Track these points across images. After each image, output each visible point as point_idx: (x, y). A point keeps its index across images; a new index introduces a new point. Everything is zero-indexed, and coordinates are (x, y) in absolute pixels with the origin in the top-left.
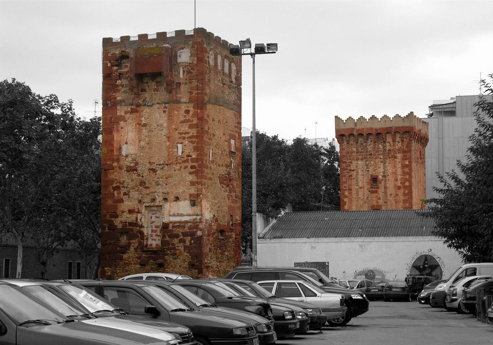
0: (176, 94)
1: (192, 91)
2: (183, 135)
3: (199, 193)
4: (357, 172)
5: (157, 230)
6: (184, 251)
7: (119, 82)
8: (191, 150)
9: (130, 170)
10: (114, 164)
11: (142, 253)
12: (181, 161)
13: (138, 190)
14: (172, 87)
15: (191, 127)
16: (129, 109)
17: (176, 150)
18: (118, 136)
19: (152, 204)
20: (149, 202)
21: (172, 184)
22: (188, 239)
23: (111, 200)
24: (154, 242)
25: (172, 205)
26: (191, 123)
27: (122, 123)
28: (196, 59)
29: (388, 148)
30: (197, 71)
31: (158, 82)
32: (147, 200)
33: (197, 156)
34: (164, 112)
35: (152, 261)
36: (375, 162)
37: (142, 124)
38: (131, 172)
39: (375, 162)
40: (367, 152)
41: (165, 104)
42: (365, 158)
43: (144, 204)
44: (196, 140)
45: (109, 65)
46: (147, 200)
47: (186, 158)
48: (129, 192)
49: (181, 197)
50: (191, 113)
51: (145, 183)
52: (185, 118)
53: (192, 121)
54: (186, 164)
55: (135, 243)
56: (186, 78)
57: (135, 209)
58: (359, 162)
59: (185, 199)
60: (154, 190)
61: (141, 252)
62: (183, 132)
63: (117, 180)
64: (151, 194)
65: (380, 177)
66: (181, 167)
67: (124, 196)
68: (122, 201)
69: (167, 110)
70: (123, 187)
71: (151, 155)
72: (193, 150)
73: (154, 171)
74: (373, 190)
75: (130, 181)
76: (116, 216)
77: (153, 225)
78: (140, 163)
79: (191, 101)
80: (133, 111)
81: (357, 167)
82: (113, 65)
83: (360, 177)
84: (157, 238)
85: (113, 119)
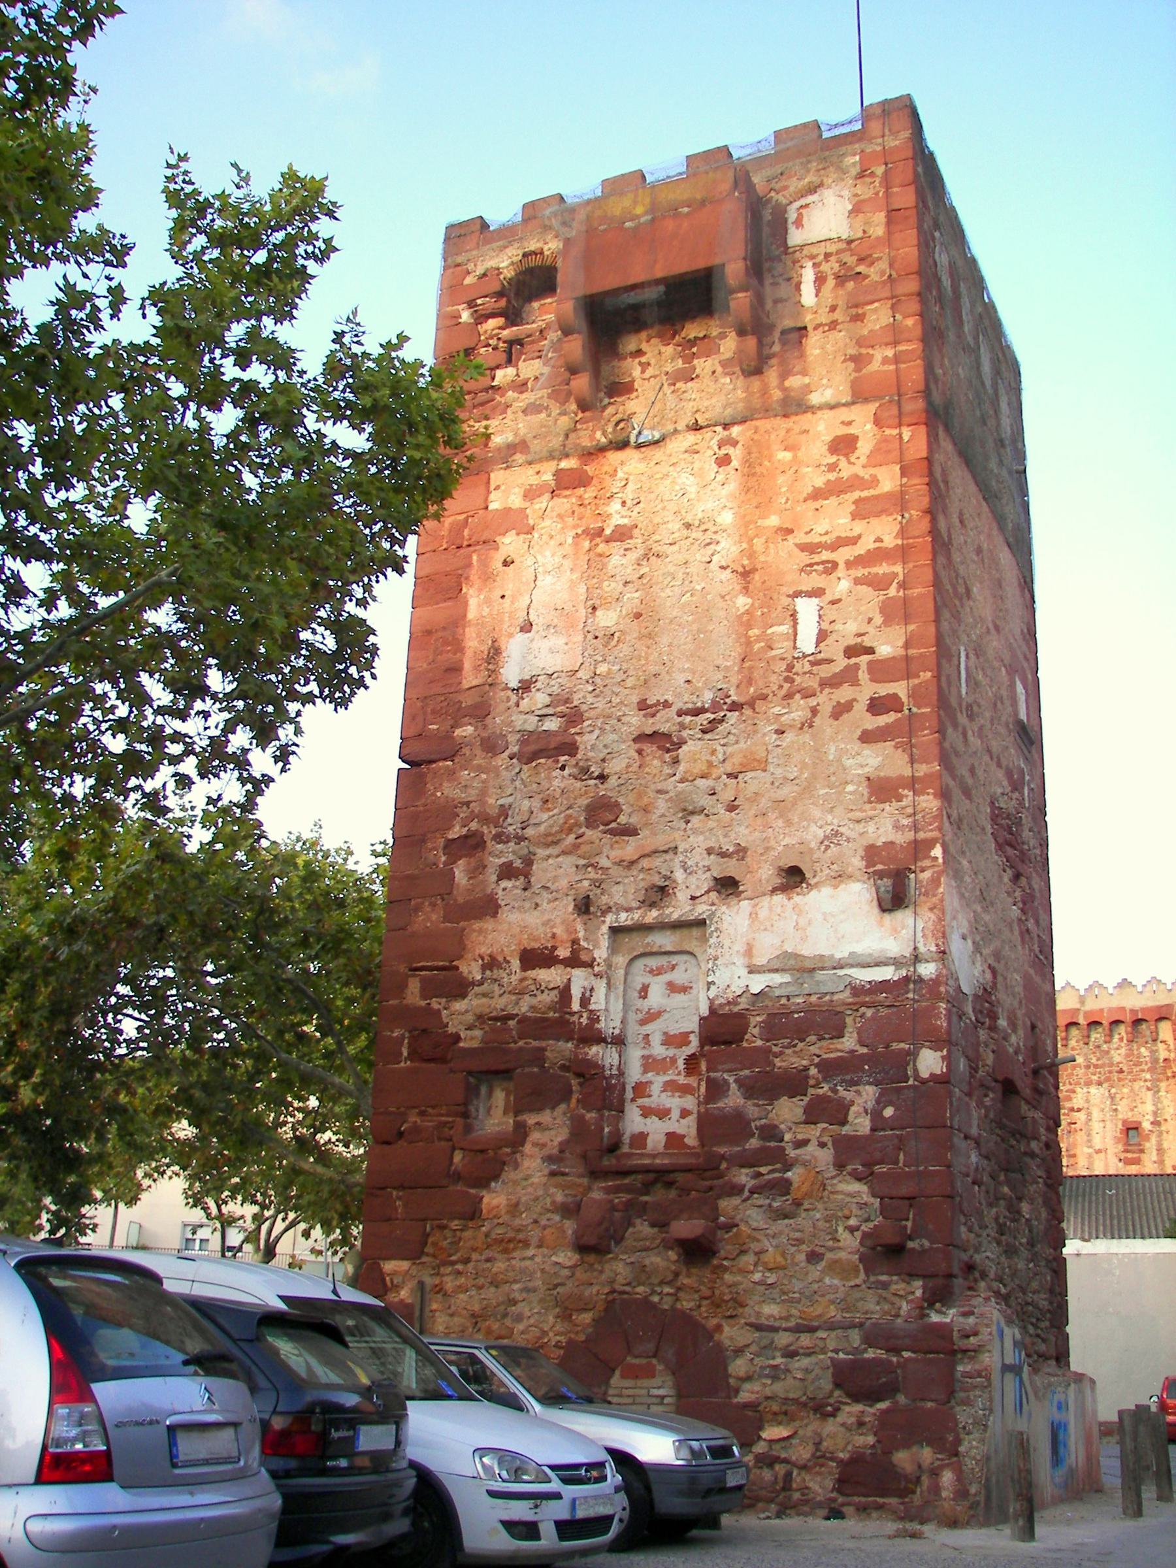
0: (784, 376)
1: (864, 351)
2: (826, 555)
3: (921, 835)
4: (1089, 1114)
5: (673, 1060)
6: (840, 1165)
7: (503, 376)
8: (870, 620)
9: (541, 751)
10: (458, 732)
11: (585, 1181)
12: (814, 683)
13: (576, 847)
14: (770, 342)
15: (861, 512)
16: (548, 477)
17: (784, 629)
18: (488, 601)
19: (652, 915)
20: (635, 904)
21: (764, 803)
22: (863, 1098)
23: (433, 905)
24: (662, 1117)
25: (763, 913)
26: (865, 494)
27: (510, 543)
28: (881, 217)
29: (1163, 1054)
30: (891, 266)
31: (693, 342)
32: (623, 898)
33: (907, 645)
34: (724, 461)
35: (642, 1228)
36: (1132, 1090)
37: (608, 532)
38: (542, 761)
39: (1132, 1090)
40: (1111, 1065)
41: (726, 426)
42: (1108, 1079)
43: (610, 919)
44: (898, 569)
45: (466, 316)
46: (623, 898)
47: (841, 663)
48: (528, 862)
49: (817, 867)
50: (864, 447)
51: (615, 808)
52: (832, 476)
53: (874, 482)
54: (844, 693)
55: (551, 1128)
56: (830, 302)
57: (554, 948)
58: (1093, 1090)
59: (840, 877)
60: (660, 841)
61: (581, 1176)
62: (823, 539)
63: (468, 804)
64: (645, 863)
65: (1146, 1125)
66: (814, 711)
67: (505, 884)
68: (489, 907)
69: (736, 453)
70: (499, 838)
71: (652, 669)
72: (878, 620)
73: (666, 742)
74: (1129, 1155)
75: (536, 803)
76: (460, 988)
77: (655, 1030)
78: (592, 714)
79: (859, 396)
80: (566, 482)
81: (1087, 1101)
82: (481, 318)
83: (1096, 1126)
84: (674, 1103)
85: (466, 532)
